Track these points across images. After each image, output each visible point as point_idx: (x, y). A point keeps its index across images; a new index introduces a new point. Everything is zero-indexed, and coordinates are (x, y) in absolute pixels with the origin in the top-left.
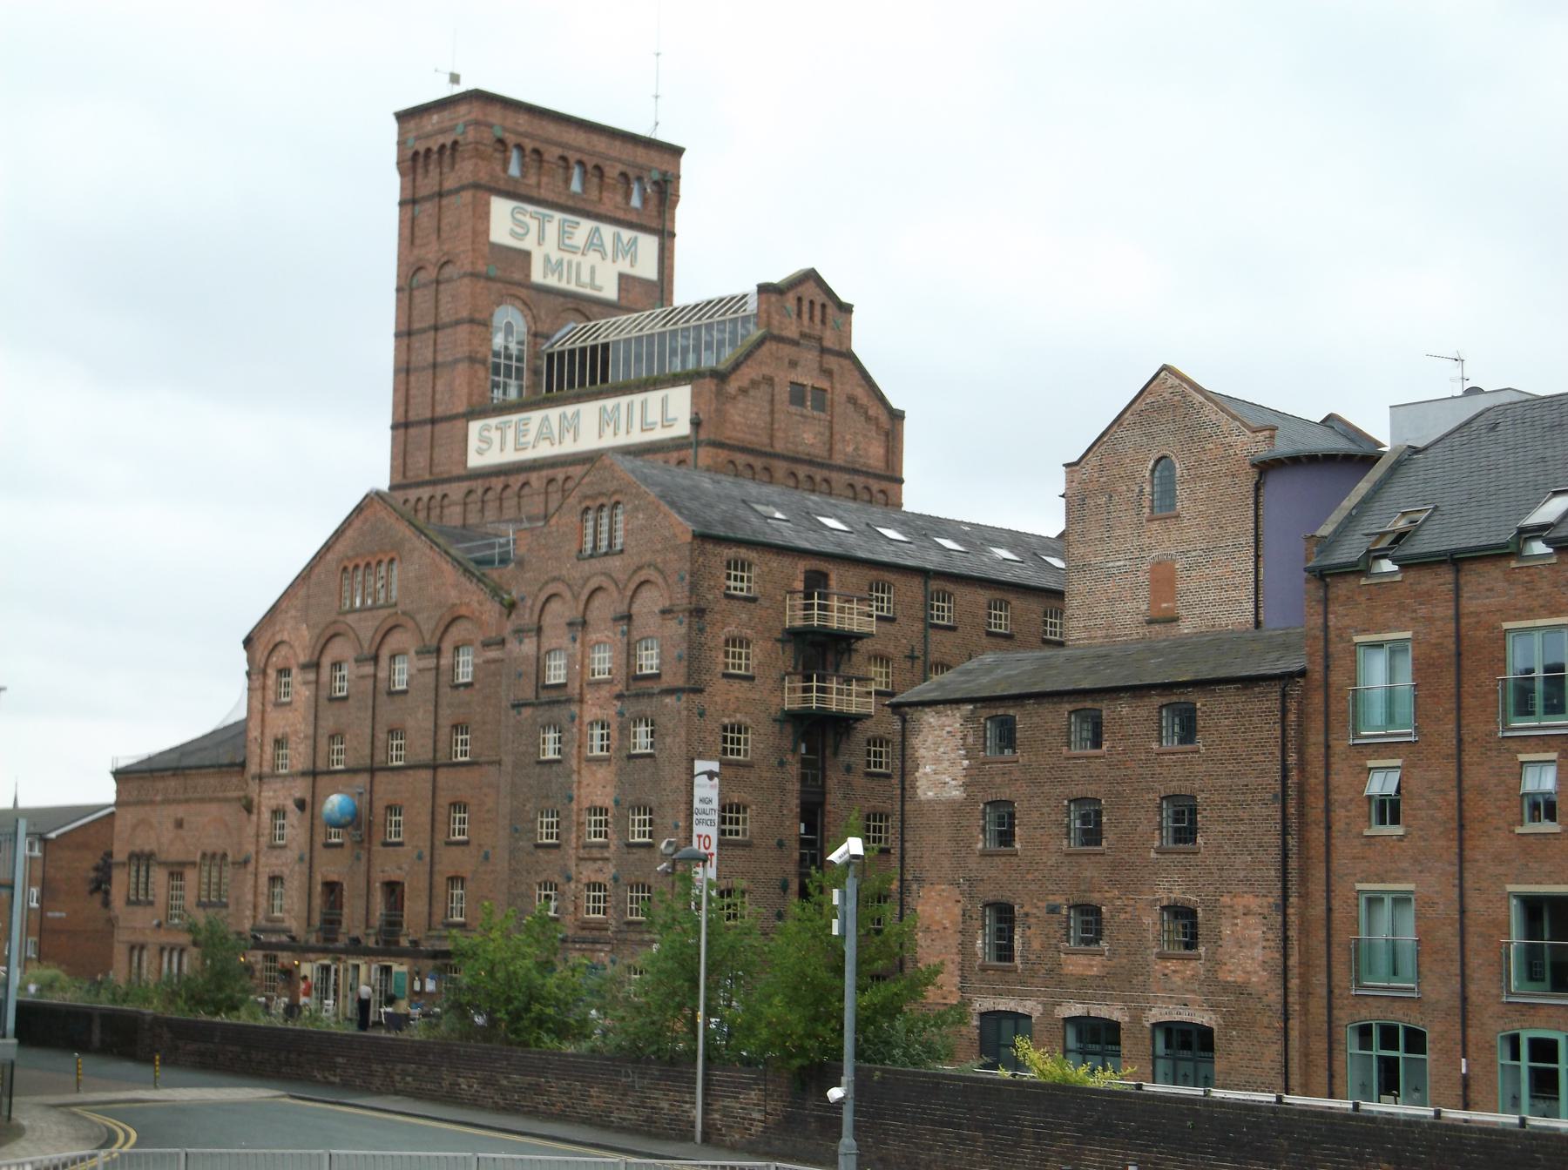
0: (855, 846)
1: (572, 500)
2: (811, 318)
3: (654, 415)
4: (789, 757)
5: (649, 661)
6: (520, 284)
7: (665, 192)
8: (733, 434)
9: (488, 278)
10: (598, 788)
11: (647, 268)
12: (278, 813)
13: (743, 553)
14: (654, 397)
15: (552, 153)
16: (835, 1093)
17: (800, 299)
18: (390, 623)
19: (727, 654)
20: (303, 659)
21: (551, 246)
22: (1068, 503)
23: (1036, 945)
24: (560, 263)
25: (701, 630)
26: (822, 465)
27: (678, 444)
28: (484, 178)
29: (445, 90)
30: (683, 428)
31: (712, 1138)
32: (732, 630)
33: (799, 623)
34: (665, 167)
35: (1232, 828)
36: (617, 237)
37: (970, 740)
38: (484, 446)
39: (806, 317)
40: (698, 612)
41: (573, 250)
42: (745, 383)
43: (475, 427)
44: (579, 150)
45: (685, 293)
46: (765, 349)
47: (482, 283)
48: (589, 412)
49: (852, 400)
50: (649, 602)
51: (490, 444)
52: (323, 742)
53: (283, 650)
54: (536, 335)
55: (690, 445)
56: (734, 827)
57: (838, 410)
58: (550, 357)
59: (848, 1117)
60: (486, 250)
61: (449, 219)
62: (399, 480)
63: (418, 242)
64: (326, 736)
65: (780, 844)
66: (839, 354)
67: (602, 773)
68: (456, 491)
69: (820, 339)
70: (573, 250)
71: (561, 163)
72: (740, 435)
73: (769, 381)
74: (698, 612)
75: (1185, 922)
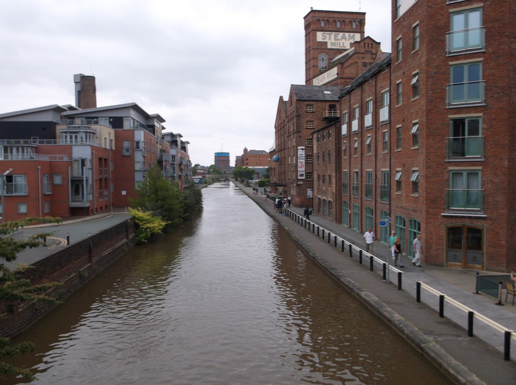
8: (345, 75)
9: (317, 49)
13: (310, 103)
17: (365, 44)
19: (307, 124)
24: (335, 43)
25: (300, 120)
28: (315, 28)
34: (361, 18)
36: (350, 35)
39: (366, 47)
40: (298, 116)
41: (338, 40)
42: (349, 64)
43: (314, 80)
46: (355, 56)
47: (315, 50)
54: (329, 59)
60: (316, 43)
69: (371, 51)
70: (338, 40)
73: (356, 63)
74: (298, 116)
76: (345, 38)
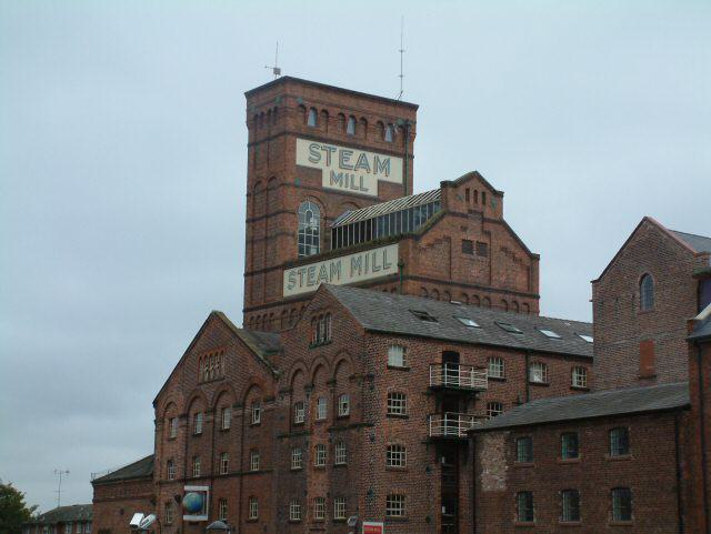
1: (307, 313)
2: (476, 201)
3: (379, 262)
4: (433, 466)
6: (316, 189)
7: (407, 132)
10: (318, 486)
11: (396, 176)
12: (168, 504)
15: (334, 112)
17: (468, 190)
18: (221, 390)
19: (389, 403)
20: (181, 412)
22: (594, 305)
24: (341, 174)
25: (372, 388)
26: (484, 289)
27: (391, 279)
29: (272, 78)
30: (394, 269)
32: (392, 388)
33: (438, 383)
35: (650, 510)
37: (509, 454)
38: (291, 284)
39: (472, 200)
41: (349, 168)
42: (431, 241)
43: (287, 273)
44: (352, 109)
49: (504, 249)
51: (295, 284)
52: (190, 460)
53: (172, 408)
54: (326, 218)
55: (397, 280)
56: (396, 509)
57: (494, 256)
58: (334, 230)
60: (294, 170)
62: (249, 306)
63: (258, 167)
64: (191, 458)
65: (428, 520)
66: (494, 222)
67: (323, 477)
68: (277, 311)
70: (349, 168)
71: (341, 117)
72: (430, 272)
76: (366, 167)
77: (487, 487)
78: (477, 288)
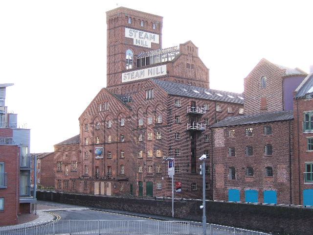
0: (204, 156)
3: (159, 71)
5: (159, 120)
7: (160, 26)
14: (159, 67)
16: (201, 207)
17: (188, 47)
20: (90, 122)
21: (137, 37)
23: (240, 176)
24: (139, 41)
26: (194, 80)
28: (123, 24)
30: (165, 73)
31: (176, 217)
45: (164, 46)
48: (146, 70)
50: (160, 108)
51: (126, 78)
59: (204, 211)
61: (117, 33)
68: (120, 87)
75: (270, 172)
77: (217, 145)
78: (191, 79)
